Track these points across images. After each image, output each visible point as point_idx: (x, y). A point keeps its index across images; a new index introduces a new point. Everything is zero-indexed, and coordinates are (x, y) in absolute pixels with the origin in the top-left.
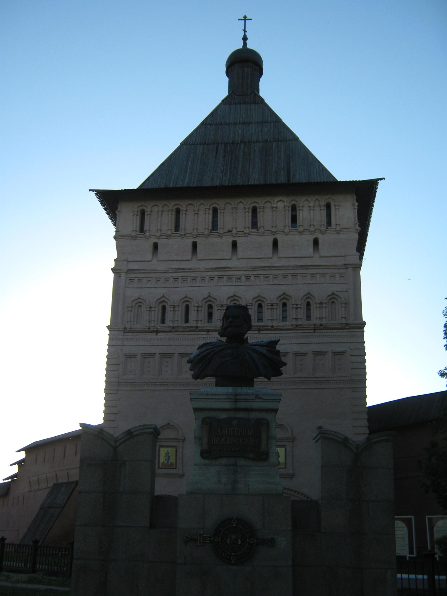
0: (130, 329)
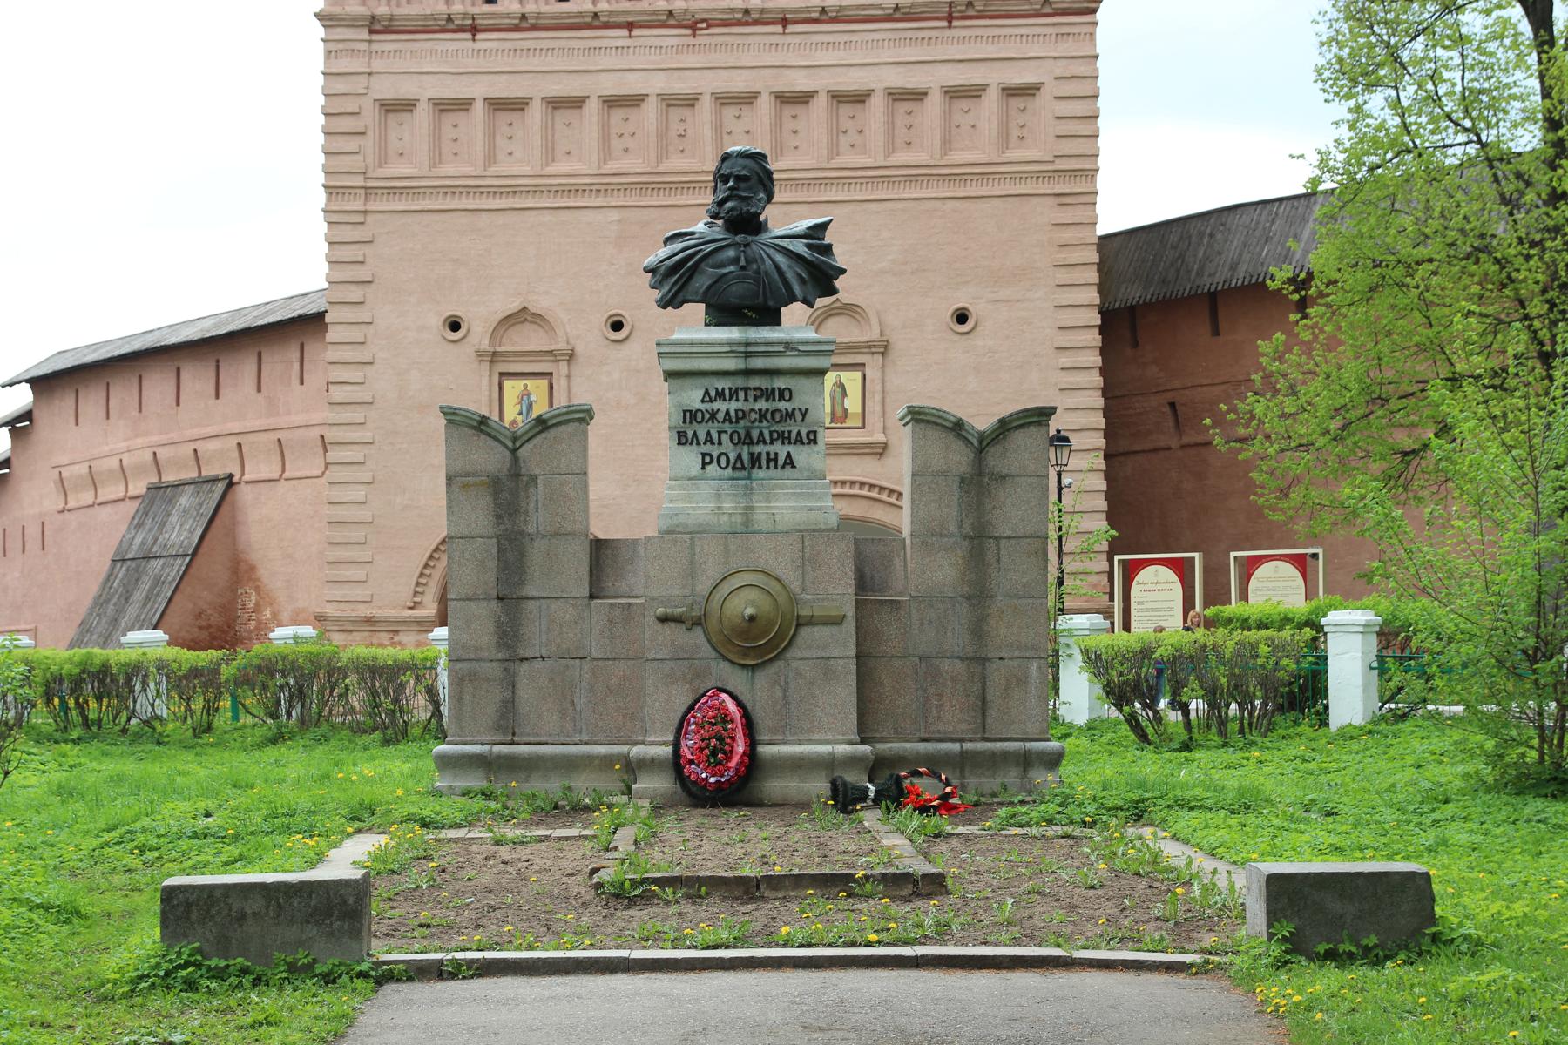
0: (391, 20)
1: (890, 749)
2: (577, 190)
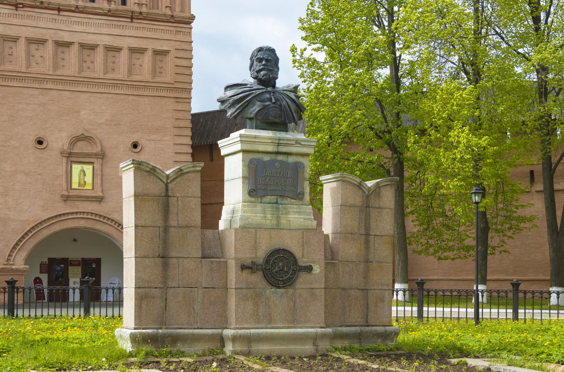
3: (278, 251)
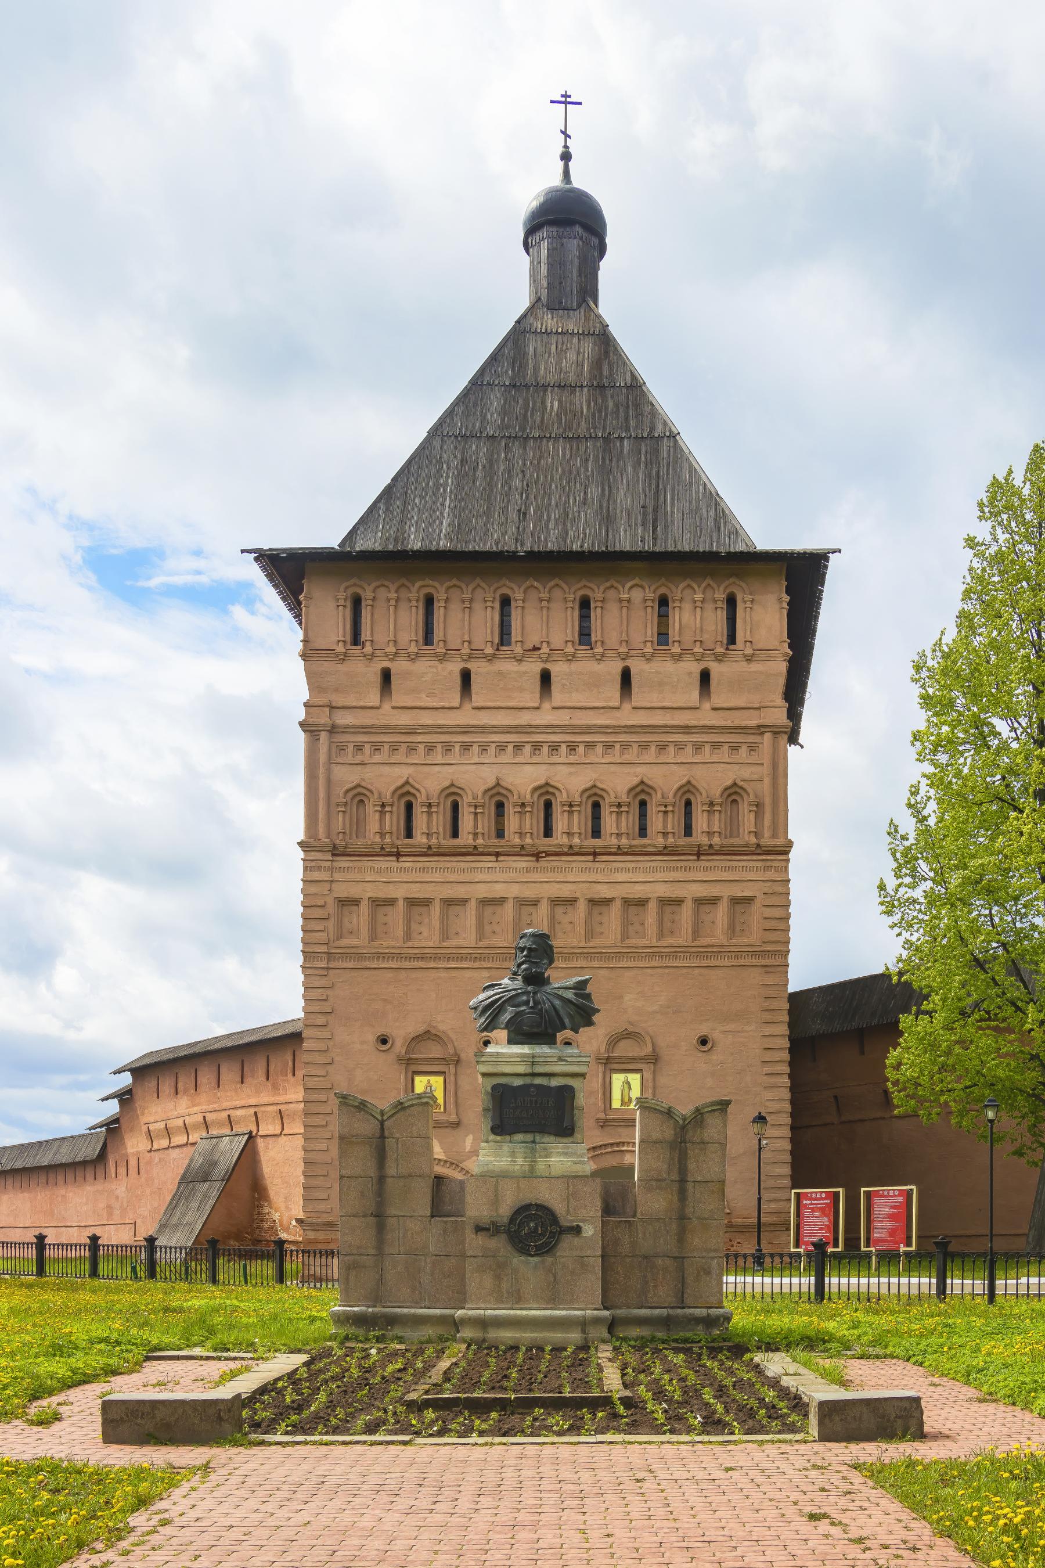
1: (534, 1332)
2: (461, 958)
3: (527, 1207)
